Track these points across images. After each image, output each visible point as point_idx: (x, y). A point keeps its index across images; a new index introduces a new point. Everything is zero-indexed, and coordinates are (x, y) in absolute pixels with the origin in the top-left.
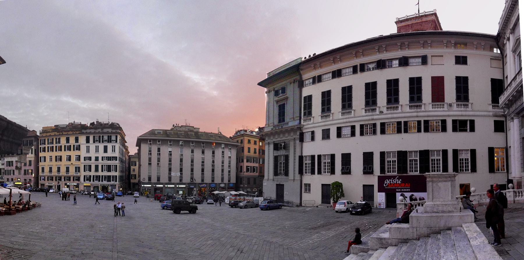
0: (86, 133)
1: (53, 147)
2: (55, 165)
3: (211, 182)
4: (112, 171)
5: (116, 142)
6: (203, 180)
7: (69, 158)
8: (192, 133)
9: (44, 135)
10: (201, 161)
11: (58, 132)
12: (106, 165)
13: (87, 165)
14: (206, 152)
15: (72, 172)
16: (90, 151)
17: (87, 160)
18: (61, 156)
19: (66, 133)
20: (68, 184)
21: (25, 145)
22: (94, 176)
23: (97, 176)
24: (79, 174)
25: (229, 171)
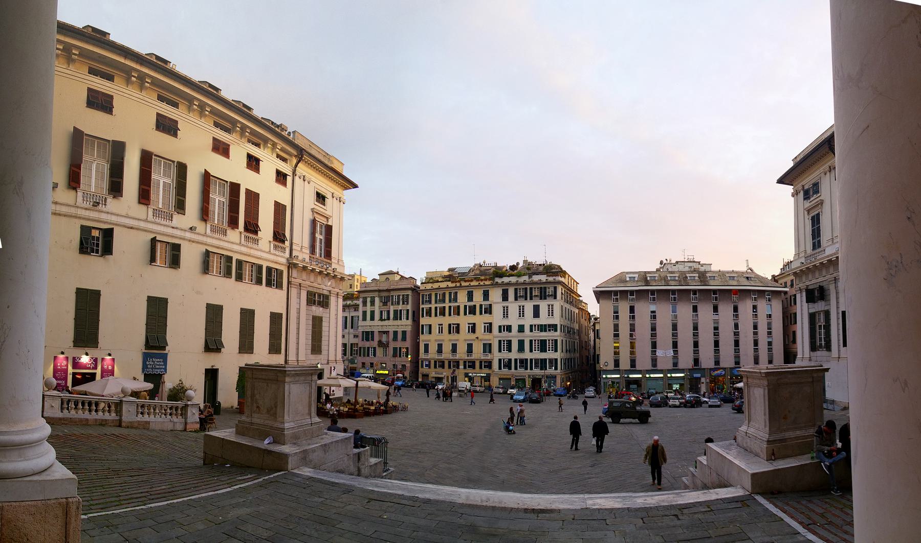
0: (503, 284)
1: (444, 307)
2: (447, 340)
3: (732, 365)
4: (549, 350)
5: (555, 298)
6: (717, 362)
7: (473, 329)
8: (694, 275)
9: (429, 286)
10: (712, 326)
11: (452, 282)
12: (538, 341)
13: (504, 341)
14: (721, 308)
15: (478, 353)
16: (509, 316)
17: (504, 331)
18: (458, 325)
19: (467, 284)
20: (470, 375)
21: (395, 304)
22: (516, 360)
23: (522, 361)
24: (489, 357)
25: (768, 342)
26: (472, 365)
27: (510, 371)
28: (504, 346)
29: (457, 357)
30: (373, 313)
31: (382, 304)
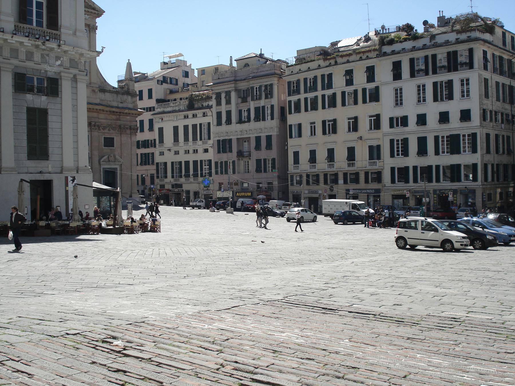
16: (404, 102)
17: (397, 125)
18: (335, 121)
24: (378, 166)
26: (356, 178)
27: (408, 185)
28: (398, 148)
29: (334, 169)
30: (229, 113)
31: (240, 100)
